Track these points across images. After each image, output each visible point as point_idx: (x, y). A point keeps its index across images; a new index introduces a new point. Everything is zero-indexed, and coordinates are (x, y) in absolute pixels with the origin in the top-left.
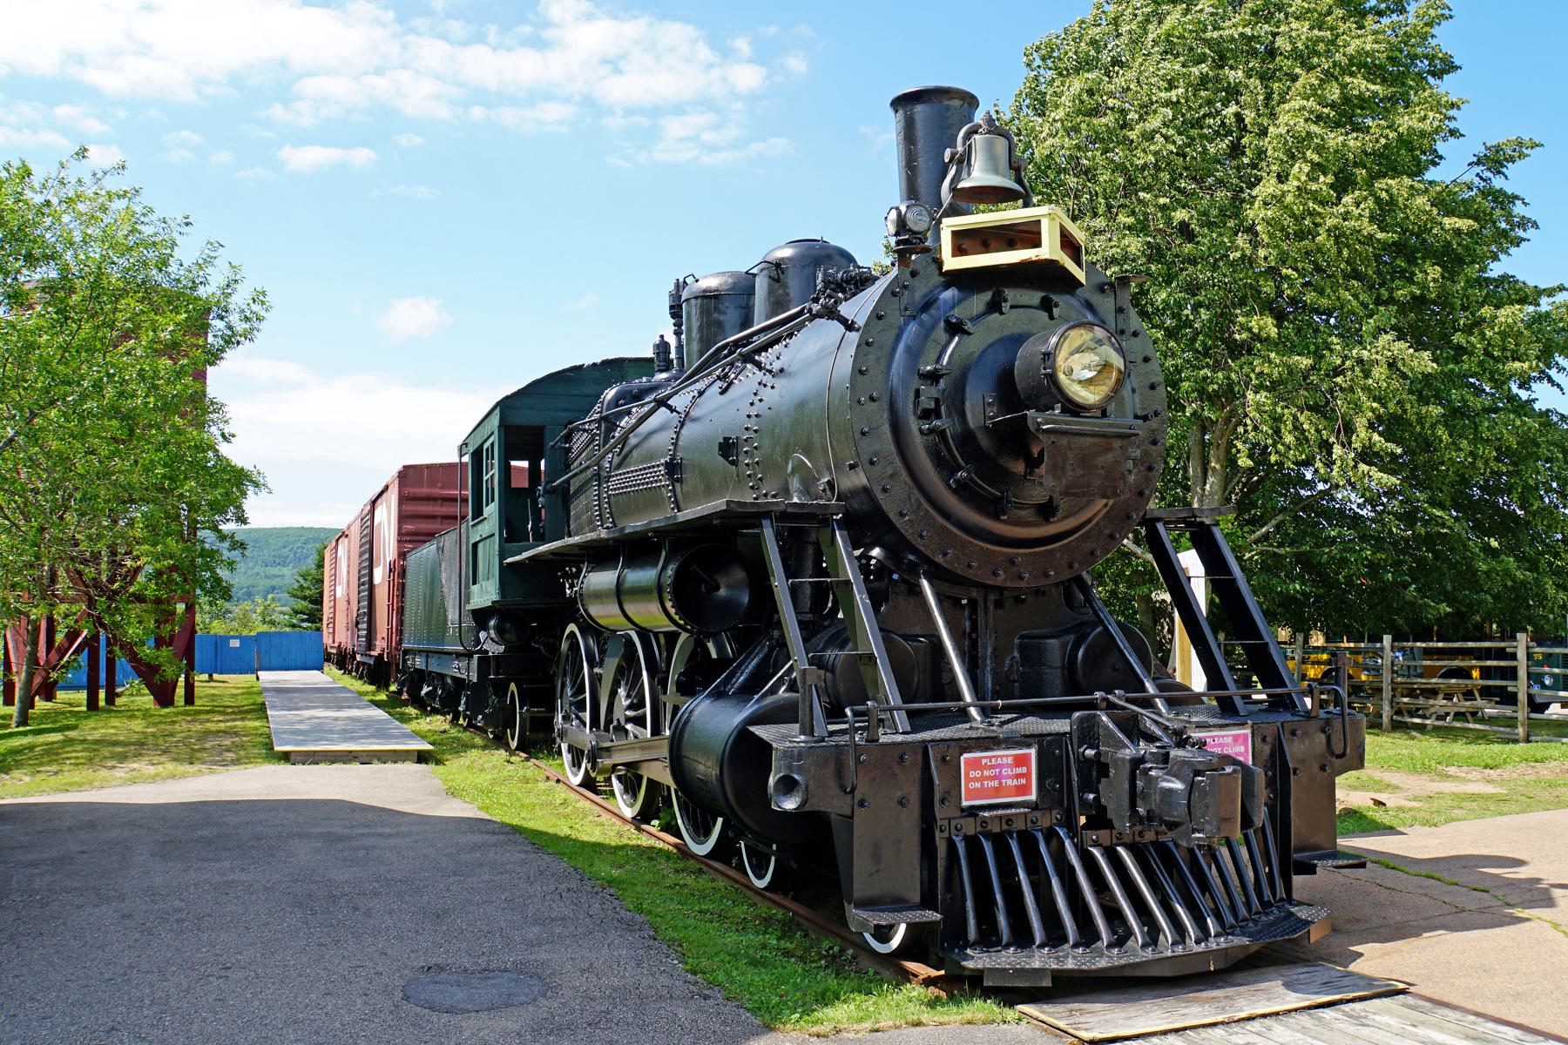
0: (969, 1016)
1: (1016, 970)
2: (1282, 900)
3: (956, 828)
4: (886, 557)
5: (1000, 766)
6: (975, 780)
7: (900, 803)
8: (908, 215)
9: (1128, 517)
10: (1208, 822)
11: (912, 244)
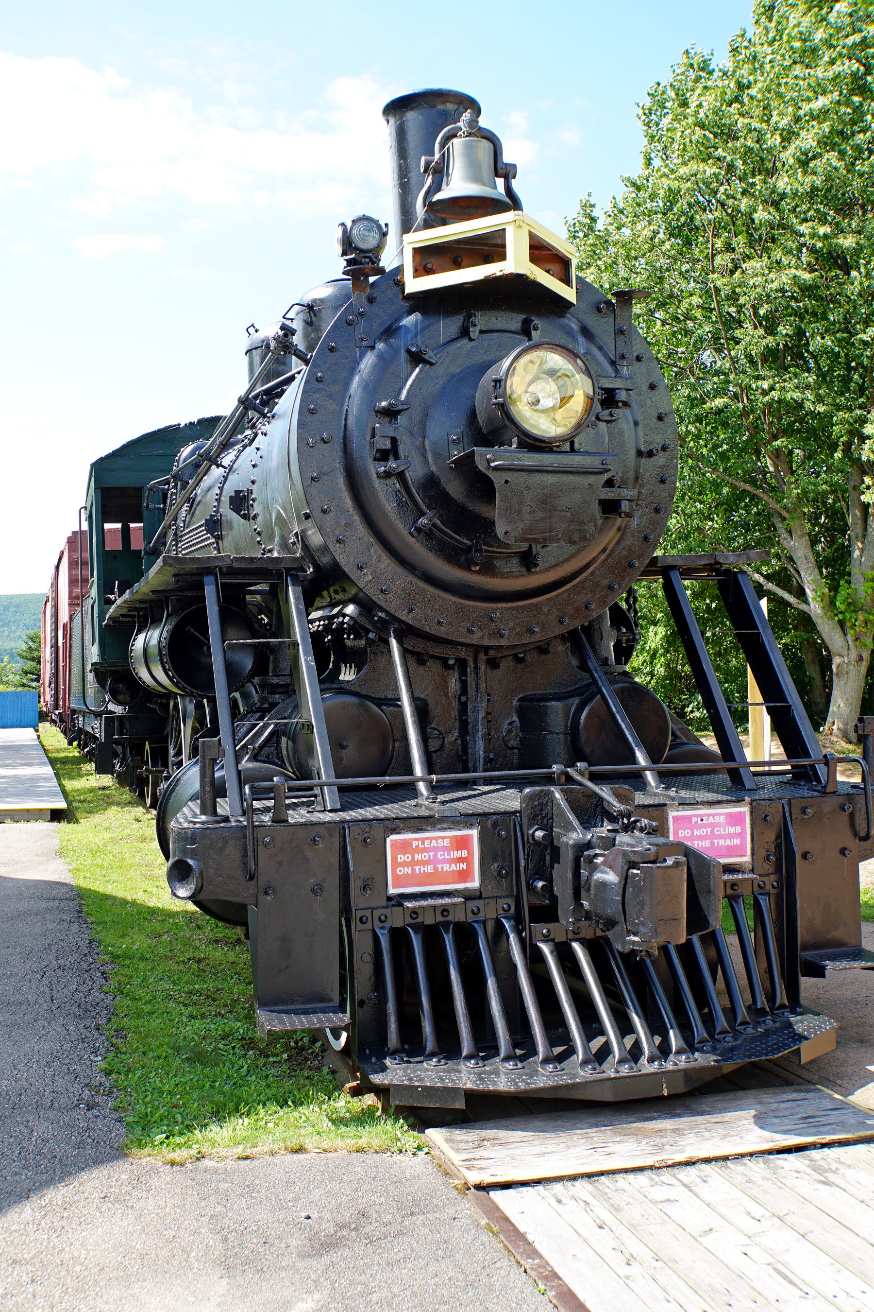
0: (363, 1142)
1: (425, 1088)
2: (782, 1006)
3: (380, 918)
4: (360, 615)
5: (435, 849)
6: (405, 864)
7: (313, 891)
8: (354, 231)
9: (631, 565)
10: (643, 923)
11: (361, 263)
